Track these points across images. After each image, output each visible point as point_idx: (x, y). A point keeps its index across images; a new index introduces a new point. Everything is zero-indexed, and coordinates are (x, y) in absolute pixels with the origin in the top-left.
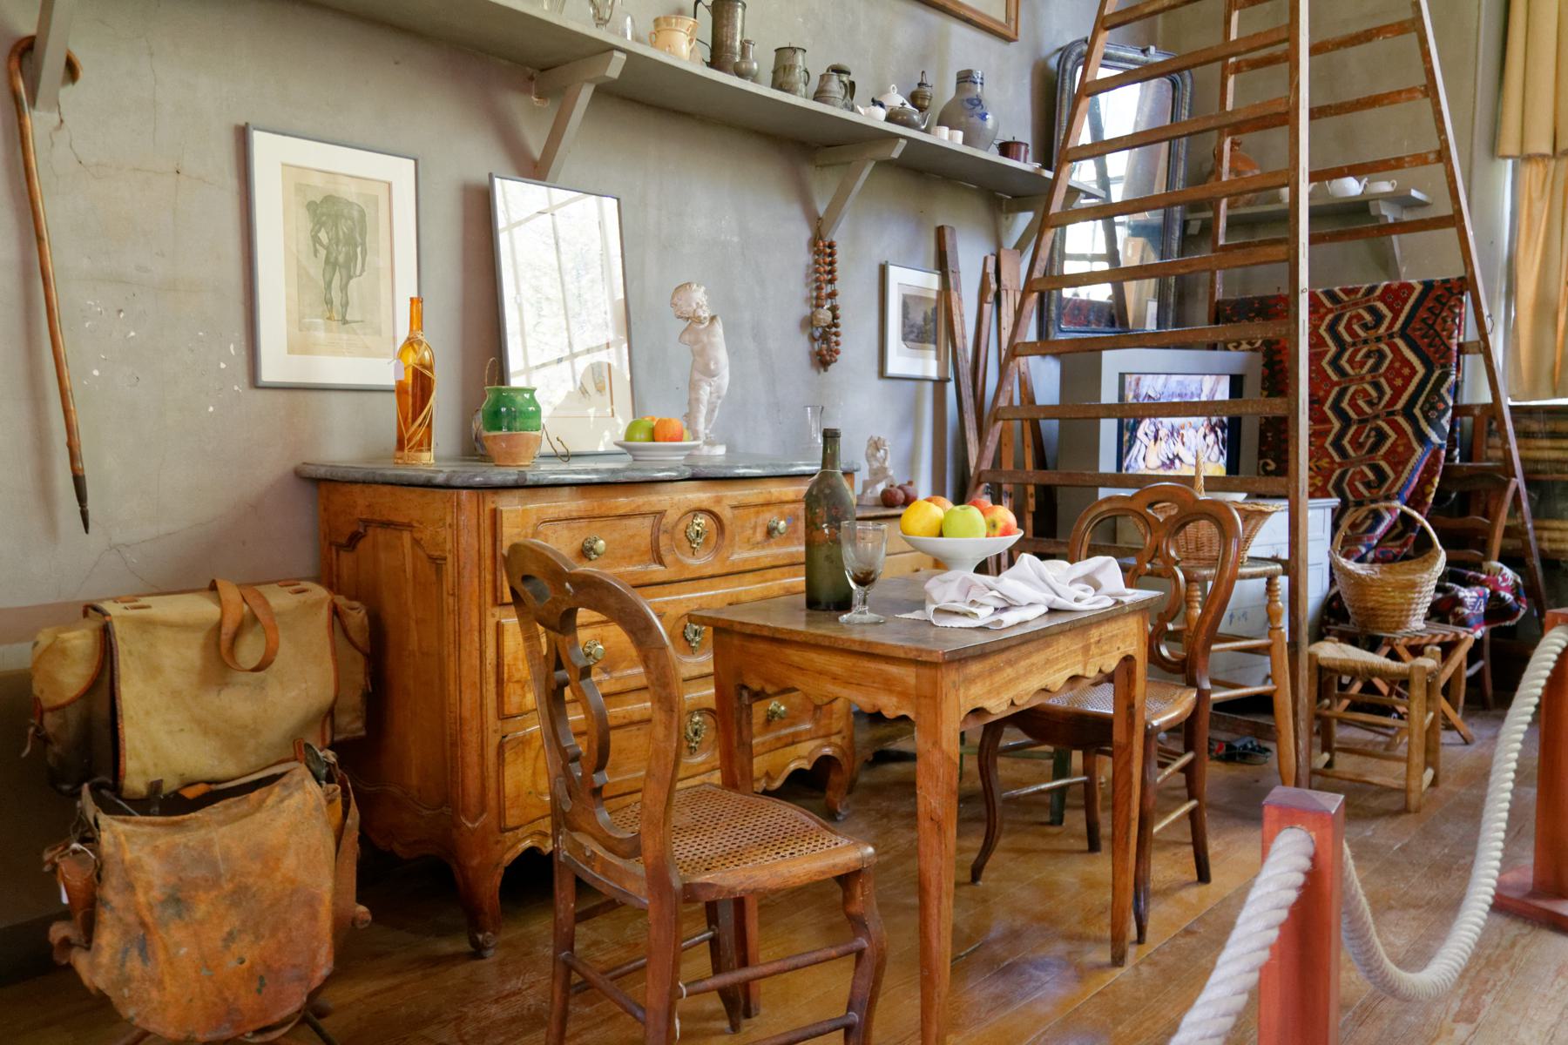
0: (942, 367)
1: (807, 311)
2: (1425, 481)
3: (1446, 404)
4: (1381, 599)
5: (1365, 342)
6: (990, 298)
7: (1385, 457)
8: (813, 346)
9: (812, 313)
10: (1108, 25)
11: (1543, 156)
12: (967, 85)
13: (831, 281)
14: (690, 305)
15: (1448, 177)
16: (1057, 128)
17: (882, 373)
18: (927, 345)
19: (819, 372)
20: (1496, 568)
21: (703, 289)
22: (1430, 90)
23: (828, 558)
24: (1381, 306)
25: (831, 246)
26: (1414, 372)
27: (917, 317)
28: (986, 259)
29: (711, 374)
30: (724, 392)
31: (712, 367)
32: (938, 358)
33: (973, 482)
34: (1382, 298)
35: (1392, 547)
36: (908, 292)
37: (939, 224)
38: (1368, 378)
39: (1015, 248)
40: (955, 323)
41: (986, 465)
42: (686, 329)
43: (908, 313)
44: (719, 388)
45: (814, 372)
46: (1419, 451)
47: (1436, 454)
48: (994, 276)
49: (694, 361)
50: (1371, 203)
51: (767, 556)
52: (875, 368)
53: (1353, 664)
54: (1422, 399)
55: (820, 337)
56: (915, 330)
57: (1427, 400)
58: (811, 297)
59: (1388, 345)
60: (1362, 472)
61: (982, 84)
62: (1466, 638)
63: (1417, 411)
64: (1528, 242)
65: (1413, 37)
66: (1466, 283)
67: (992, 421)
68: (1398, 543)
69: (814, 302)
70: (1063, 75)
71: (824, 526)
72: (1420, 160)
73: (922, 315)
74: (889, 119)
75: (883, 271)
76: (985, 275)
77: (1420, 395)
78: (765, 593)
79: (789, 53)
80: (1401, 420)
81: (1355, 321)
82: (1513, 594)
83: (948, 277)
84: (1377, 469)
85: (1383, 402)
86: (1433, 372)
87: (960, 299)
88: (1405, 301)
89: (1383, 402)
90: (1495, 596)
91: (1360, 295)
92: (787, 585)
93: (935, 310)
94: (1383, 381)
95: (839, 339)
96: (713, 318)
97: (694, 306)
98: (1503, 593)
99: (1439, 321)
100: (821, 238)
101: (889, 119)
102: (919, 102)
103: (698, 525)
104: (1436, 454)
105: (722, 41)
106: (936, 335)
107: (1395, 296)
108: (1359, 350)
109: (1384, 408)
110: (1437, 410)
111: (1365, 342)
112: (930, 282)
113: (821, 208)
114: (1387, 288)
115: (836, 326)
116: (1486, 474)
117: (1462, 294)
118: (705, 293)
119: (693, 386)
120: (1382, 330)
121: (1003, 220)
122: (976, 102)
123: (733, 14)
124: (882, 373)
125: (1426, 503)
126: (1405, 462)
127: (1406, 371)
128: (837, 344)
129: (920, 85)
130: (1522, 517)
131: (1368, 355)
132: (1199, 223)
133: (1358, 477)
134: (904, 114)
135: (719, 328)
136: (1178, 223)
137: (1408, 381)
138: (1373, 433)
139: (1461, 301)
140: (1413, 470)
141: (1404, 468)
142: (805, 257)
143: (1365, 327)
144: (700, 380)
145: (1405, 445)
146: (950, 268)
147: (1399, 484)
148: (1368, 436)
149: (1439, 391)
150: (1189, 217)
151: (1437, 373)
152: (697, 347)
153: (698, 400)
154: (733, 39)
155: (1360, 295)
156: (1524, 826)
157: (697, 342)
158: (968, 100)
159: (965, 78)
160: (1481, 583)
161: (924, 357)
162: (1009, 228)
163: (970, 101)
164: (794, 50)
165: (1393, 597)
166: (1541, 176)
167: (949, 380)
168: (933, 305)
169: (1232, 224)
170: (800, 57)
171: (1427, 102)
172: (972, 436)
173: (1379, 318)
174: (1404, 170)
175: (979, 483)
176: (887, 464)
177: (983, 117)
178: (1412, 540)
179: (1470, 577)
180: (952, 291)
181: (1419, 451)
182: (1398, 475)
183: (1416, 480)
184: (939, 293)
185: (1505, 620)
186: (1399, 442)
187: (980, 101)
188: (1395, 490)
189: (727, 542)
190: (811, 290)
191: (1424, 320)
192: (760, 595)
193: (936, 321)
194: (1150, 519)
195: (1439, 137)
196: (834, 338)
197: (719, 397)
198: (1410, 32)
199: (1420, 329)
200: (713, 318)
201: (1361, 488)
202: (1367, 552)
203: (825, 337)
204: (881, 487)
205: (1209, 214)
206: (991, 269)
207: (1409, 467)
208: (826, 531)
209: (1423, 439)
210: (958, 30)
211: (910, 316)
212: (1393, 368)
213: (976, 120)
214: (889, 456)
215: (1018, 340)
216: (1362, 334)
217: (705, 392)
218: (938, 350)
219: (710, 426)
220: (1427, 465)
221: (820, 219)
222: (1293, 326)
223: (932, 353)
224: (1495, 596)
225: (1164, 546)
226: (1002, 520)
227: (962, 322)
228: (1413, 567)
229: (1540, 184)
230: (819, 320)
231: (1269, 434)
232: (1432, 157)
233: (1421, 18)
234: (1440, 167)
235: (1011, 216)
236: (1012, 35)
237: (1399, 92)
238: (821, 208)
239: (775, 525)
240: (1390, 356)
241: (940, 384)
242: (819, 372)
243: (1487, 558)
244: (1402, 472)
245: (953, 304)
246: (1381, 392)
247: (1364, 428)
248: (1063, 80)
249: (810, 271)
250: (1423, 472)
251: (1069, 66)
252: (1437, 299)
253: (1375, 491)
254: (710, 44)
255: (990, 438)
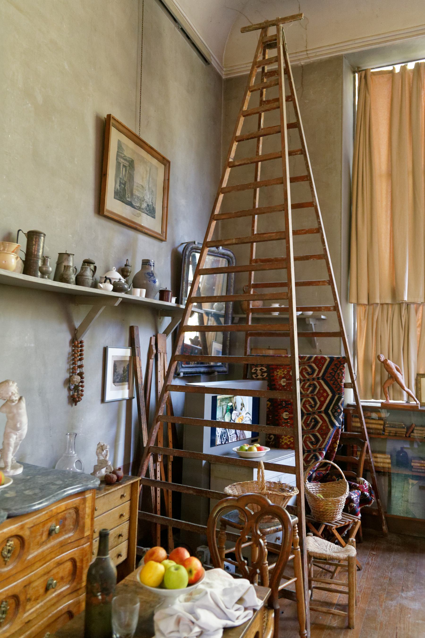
0: (131, 392)
1: (68, 376)
2: (334, 442)
3: (341, 410)
4: (326, 508)
5: (308, 380)
6: (153, 357)
7: (318, 431)
8: (69, 393)
9: (71, 377)
10: (209, 246)
11: (364, 304)
12: (147, 266)
13: (81, 360)
14: (8, 394)
15: (338, 317)
16: (182, 279)
17: (103, 400)
18: (124, 383)
19: (72, 406)
20: (362, 481)
21: (16, 384)
22: (331, 282)
23: (100, 614)
24: (314, 365)
25: (81, 342)
26: (328, 395)
27: (120, 370)
28: (151, 338)
29: (16, 429)
30: (24, 437)
31: (18, 425)
32: (129, 388)
33: (146, 451)
34: (314, 362)
35: (322, 471)
36: (116, 359)
37: (131, 325)
38: (310, 396)
39: (164, 333)
40: (138, 372)
41: (152, 445)
42: (4, 405)
43: (116, 369)
44: (21, 435)
45: (70, 406)
46: (332, 429)
47: (337, 431)
48: (154, 346)
49: (8, 422)
50: (307, 319)
51: (48, 549)
52: (100, 398)
53: (324, 556)
54: (331, 407)
55: (74, 388)
56: (119, 377)
57: (333, 408)
58: (70, 369)
59: (317, 382)
60: (309, 437)
61: (153, 266)
62: (358, 521)
63: (330, 412)
64: (360, 337)
65: (324, 261)
66: (346, 359)
67: (155, 422)
68: (324, 469)
69: (71, 371)
70: (185, 257)
71: (99, 594)
72: (328, 309)
73: (122, 369)
74: (114, 290)
75: (105, 350)
76: (150, 346)
77: (331, 405)
78: (46, 570)
79: (65, 256)
80: (324, 415)
81: (304, 371)
82: (369, 493)
83: (135, 349)
84: (315, 436)
85: (317, 407)
86: (335, 396)
87: (140, 360)
88: (323, 365)
89: (317, 407)
90: (363, 494)
91: (305, 360)
92: (58, 560)
93: (129, 366)
94: (316, 397)
95: (83, 388)
96: (20, 399)
97: (10, 394)
98: (366, 493)
99: (336, 374)
100: (76, 340)
101: (114, 290)
102: (125, 273)
103: (9, 546)
104: (337, 431)
105: (32, 252)
106: (128, 377)
107: (320, 361)
108: (306, 383)
109: (317, 410)
110: (338, 413)
111: (308, 380)
112: (126, 353)
113: (77, 324)
114: (316, 357)
115: (82, 386)
116: (354, 438)
117: (344, 364)
118: (17, 386)
119: (6, 436)
120: (315, 375)
121: (159, 319)
122: (151, 275)
123: (39, 239)
124: (103, 400)
125: (335, 452)
126: (326, 434)
127: (325, 394)
128: (82, 391)
129: (126, 265)
130: (369, 457)
131: (310, 386)
132: (238, 318)
133: (308, 439)
134: (120, 285)
135: (23, 404)
136: (230, 318)
137: (326, 398)
138: (313, 421)
139: (344, 367)
140: (330, 438)
141: (326, 437)
142: (68, 349)
143: (308, 374)
144: (11, 432)
145: (325, 426)
146: (136, 346)
147: (324, 444)
148: (311, 421)
149: (338, 404)
150: (234, 316)
151: (337, 397)
152: (10, 415)
153: (9, 444)
154: (38, 251)
155: (305, 360)
156: (397, 633)
157: (10, 412)
158: (147, 273)
159: (146, 263)
160: (357, 488)
161: (123, 389)
162: (161, 323)
163: (148, 274)
164: (69, 255)
165: (331, 507)
166: (364, 311)
167: (134, 398)
168: (128, 363)
169: (253, 319)
170: (71, 258)
171: (330, 287)
172: (144, 426)
173: (313, 370)
174: (321, 312)
175: (148, 453)
176: (107, 458)
177: (155, 282)
178: (330, 468)
179: (353, 485)
180: (137, 357)
181: (332, 429)
182: (324, 441)
183: (331, 442)
184: (130, 357)
185: (367, 504)
186: (323, 425)
187: (153, 274)
188: (323, 446)
189: (25, 550)
190: (70, 365)
191: (331, 373)
192: (43, 573)
193: (128, 371)
194: (247, 513)
195: (335, 301)
196: (80, 388)
197: (20, 440)
198: (322, 259)
199: (330, 377)
200: (20, 399)
201: (310, 445)
202: (313, 474)
203: (76, 388)
204: (103, 471)
205: (245, 316)
206: (153, 343)
207: (328, 437)
208: (100, 597)
209: (333, 425)
210: (142, 238)
211: (117, 371)
212: (320, 393)
213: (152, 283)
214: (108, 454)
215: (168, 384)
216: (307, 377)
217: (13, 439)
218: (129, 384)
219: (14, 454)
220: (334, 435)
221: (76, 329)
222: (294, 395)
223: (126, 386)
224: (363, 494)
225: (255, 531)
226: (196, 569)
227: (141, 368)
228: (333, 485)
229: (364, 313)
230: (74, 382)
231: (270, 416)
232: (332, 308)
233: (327, 254)
234: (335, 313)
235: (162, 317)
236: (164, 239)
237: (319, 282)
238: (77, 324)
239: (53, 528)
240: (318, 387)
241: (129, 401)
242: (72, 406)
243: (358, 476)
244: (325, 439)
245: (137, 363)
246: (316, 403)
247: (310, 417)
248: (185, 259)
249: (70, 355)
250: (333, 438)
251: (187, 253)
252: (335, 365)
253: (315, 446)
254: (25, 252)
255: (154, 431)
